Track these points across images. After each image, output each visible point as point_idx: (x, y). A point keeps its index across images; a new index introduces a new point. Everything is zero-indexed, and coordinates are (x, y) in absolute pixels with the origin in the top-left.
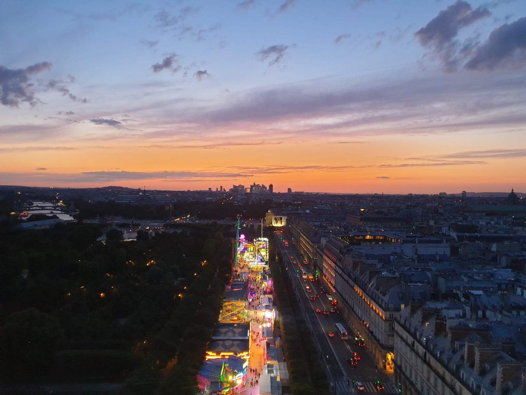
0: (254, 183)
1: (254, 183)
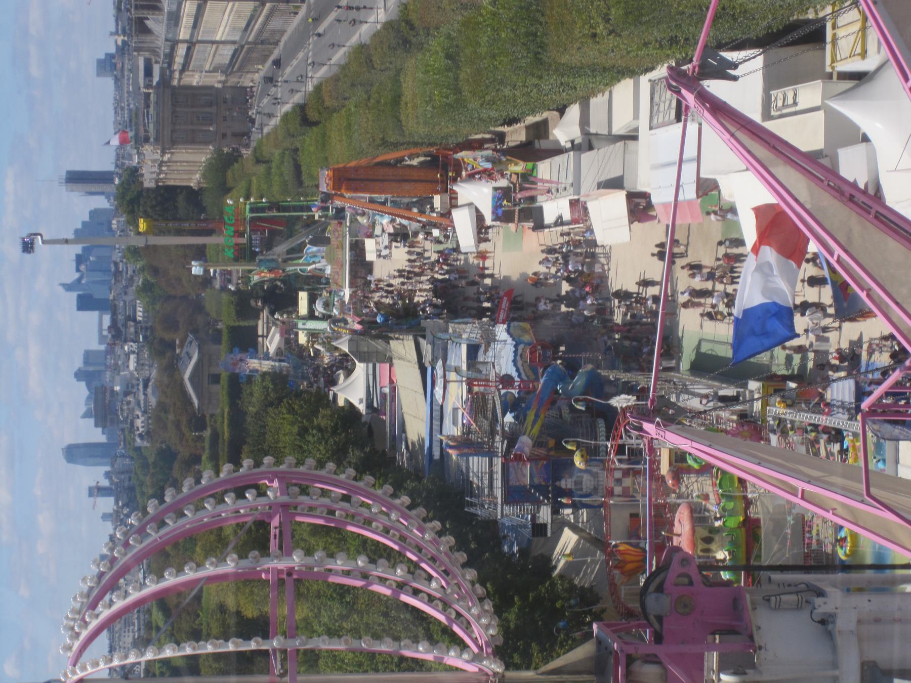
0: (68, 287)
1: (68, 287)
